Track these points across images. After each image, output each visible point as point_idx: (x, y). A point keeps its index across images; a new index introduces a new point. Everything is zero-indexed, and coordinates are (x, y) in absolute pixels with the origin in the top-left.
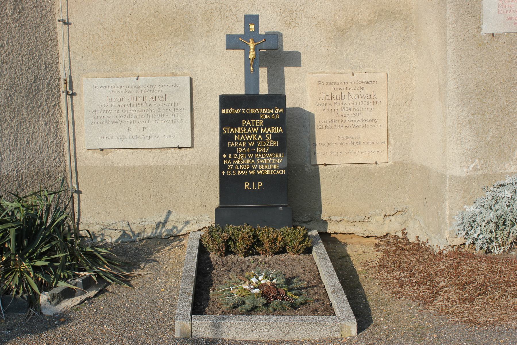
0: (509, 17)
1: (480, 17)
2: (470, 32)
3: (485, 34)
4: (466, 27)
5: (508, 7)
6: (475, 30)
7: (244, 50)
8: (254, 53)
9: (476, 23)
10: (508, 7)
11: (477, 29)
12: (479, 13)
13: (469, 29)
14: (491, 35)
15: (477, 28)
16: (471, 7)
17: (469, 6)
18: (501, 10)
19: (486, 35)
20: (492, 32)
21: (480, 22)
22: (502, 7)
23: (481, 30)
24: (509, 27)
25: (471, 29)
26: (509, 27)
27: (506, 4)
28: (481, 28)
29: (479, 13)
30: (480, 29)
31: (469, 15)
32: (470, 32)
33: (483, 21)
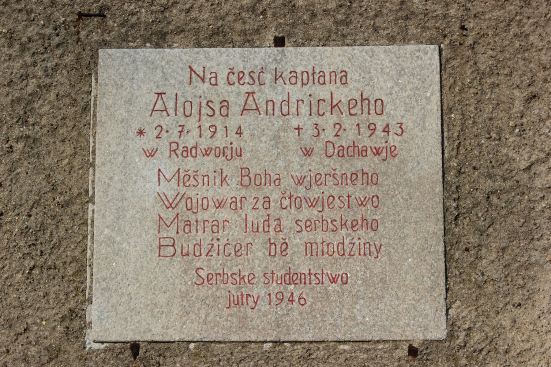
0: (203, 273)
1: (81, 271)
2: (32, 338)
3: (102, 346)
4: (15, 314)
5: (200, 229)
6: (54, 328)
7: (98, 49)
8: (96, 348)
9: (62, 296)
10: (200, 229)
11: (66, 324)
12: (77, 253)
13: (30, 321)
14: (128, 353)
15: (63, 319)
16: (43, 227)
17: (32, 222)
18: (169, 242)
19: (105, 351)
20: (130, 337)
21: (80, 290)
22: (174, 226)
23: (81, 329)
24: (207, 315)
25: (39, 325)
26: (207, 315)
27: (192, 218)
28: (83, 317)
29: (77, 253)
30: (76, 324)
31: (29, 263)
32: (32, 338)
33: (91, 287)
